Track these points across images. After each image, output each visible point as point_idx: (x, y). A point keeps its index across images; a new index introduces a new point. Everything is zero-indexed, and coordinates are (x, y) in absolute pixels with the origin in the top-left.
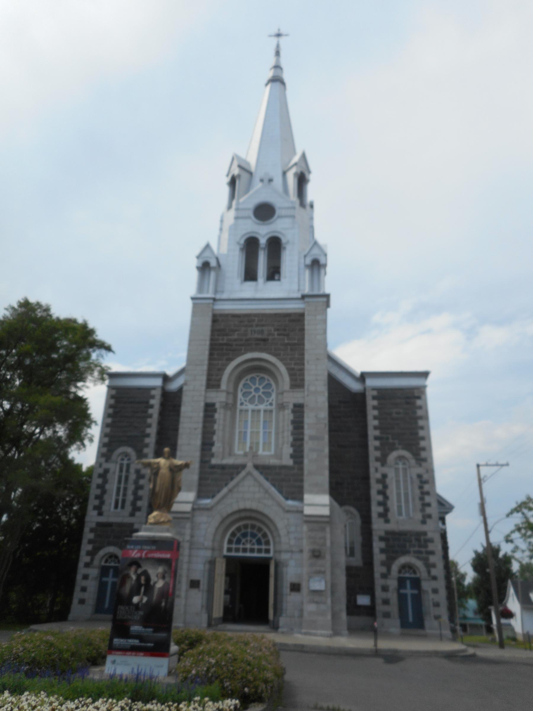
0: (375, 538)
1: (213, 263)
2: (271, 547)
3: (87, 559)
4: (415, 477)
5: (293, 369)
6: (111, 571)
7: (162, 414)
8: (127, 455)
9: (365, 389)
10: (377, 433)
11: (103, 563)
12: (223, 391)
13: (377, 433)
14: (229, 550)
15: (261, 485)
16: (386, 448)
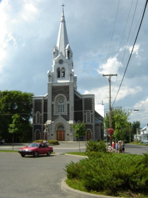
1: (51, 75)
3: (34, 131)
7: (44, 104)
8: (38, 113)
10: (84, 107)
13: (84, 107)
16: (86, 109)
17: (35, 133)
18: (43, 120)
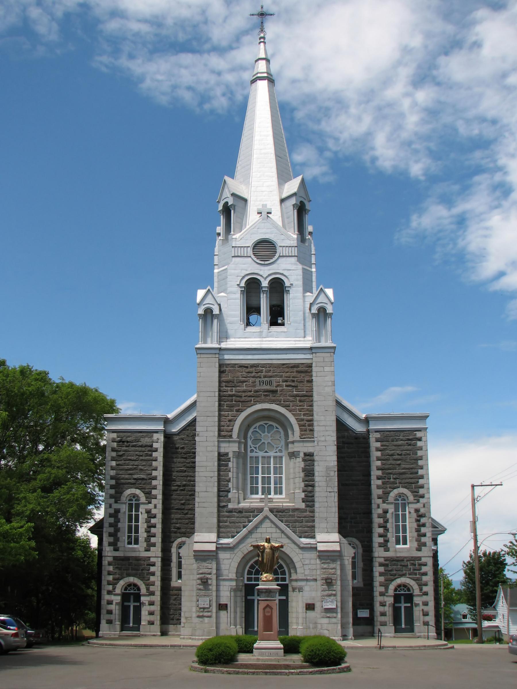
0: (376, 564)
1: (216, 311)
2: (287, 576)
4: (412, 511)
5: (302, 420)
6: (132, 597)
9: (368, 431)
11: (123, 591)
12: (234, 442)
14: (249, 579)
15: (277, 527)
16: (388, 485)
17: (390, 600)
18: (158, 531)
